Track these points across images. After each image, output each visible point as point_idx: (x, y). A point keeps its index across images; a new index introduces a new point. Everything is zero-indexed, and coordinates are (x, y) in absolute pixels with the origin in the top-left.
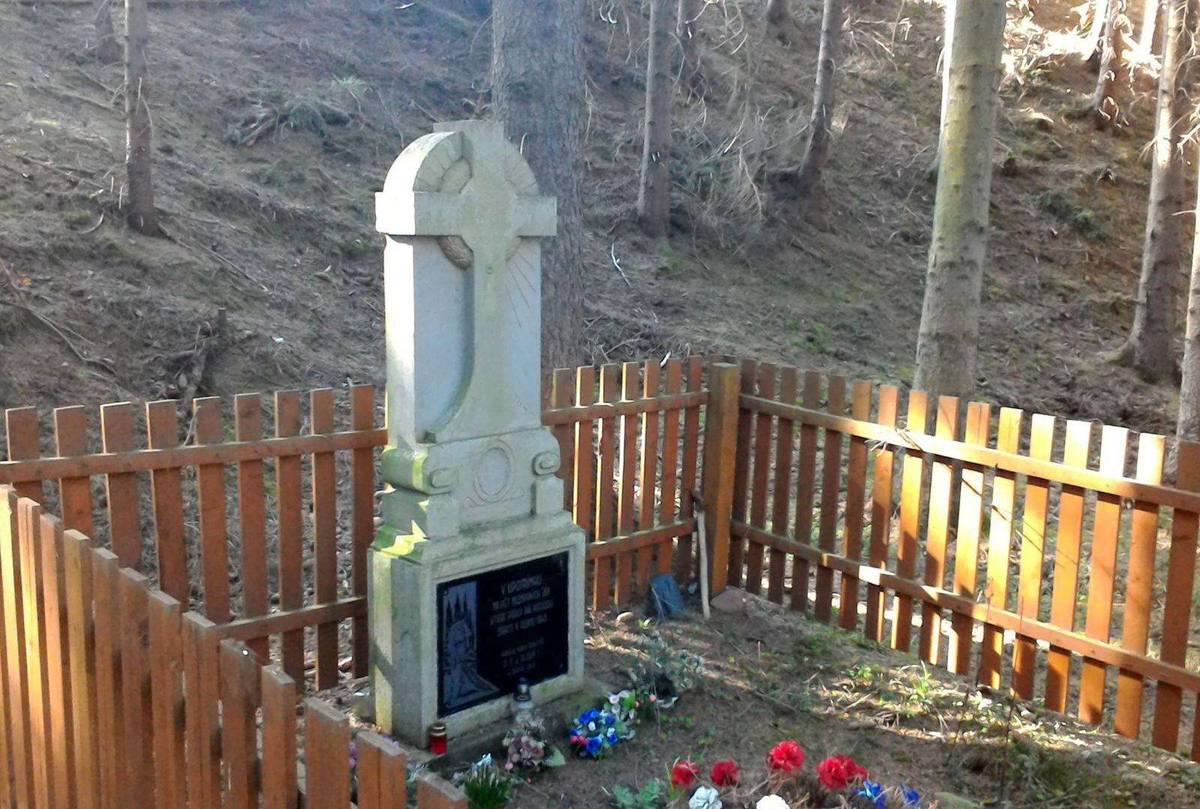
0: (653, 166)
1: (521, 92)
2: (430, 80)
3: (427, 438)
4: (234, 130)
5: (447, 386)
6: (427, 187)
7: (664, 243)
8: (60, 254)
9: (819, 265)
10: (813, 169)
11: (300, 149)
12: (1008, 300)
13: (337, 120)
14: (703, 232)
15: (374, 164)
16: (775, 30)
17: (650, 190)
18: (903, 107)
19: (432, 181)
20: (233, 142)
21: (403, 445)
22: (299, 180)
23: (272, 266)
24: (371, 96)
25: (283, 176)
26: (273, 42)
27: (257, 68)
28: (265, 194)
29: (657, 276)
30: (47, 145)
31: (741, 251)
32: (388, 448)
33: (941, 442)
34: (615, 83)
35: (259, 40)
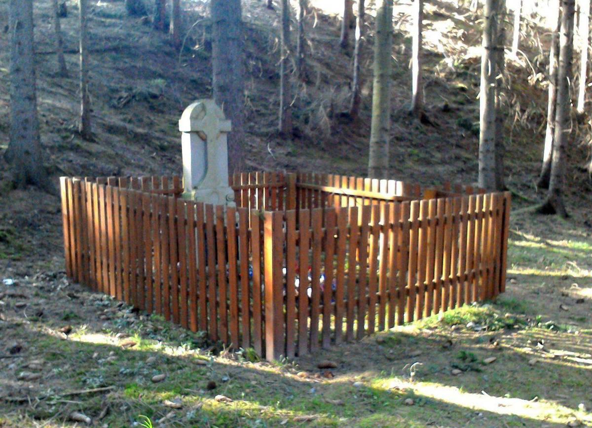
0: (285, 112)
1: (223, 89)
2: (192, 78)
3: (195, 188)
4: (115, 102)
5: (200, 175)
6: (194, 118)
7: (289, 142)
8: (61, 149)
9: (356, 150)
10: (355, 111)
11: (140, 108)
12: (439, 164)
13: (155, 97)
14: (306, 137)
15: (170, 114)
16: (344, 51)
17: (284, 121)
18: (400, 83)
19: (194, 116)
20: (114, 107)
21: (188, 190)
22: (141, 121)
23: (134, 153)
24: (168, 86)
25: (134, 119)
26: (127, 65)
27: (121, 77)
28: (129, 126)
29: (287, 155)
30: (49, 110)
31: (323, 144)
32: (184, 192)
33: (351, 191)
34: (271, 78)
35: (121, 65)
